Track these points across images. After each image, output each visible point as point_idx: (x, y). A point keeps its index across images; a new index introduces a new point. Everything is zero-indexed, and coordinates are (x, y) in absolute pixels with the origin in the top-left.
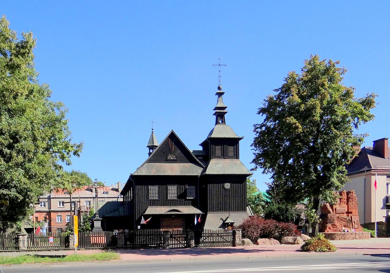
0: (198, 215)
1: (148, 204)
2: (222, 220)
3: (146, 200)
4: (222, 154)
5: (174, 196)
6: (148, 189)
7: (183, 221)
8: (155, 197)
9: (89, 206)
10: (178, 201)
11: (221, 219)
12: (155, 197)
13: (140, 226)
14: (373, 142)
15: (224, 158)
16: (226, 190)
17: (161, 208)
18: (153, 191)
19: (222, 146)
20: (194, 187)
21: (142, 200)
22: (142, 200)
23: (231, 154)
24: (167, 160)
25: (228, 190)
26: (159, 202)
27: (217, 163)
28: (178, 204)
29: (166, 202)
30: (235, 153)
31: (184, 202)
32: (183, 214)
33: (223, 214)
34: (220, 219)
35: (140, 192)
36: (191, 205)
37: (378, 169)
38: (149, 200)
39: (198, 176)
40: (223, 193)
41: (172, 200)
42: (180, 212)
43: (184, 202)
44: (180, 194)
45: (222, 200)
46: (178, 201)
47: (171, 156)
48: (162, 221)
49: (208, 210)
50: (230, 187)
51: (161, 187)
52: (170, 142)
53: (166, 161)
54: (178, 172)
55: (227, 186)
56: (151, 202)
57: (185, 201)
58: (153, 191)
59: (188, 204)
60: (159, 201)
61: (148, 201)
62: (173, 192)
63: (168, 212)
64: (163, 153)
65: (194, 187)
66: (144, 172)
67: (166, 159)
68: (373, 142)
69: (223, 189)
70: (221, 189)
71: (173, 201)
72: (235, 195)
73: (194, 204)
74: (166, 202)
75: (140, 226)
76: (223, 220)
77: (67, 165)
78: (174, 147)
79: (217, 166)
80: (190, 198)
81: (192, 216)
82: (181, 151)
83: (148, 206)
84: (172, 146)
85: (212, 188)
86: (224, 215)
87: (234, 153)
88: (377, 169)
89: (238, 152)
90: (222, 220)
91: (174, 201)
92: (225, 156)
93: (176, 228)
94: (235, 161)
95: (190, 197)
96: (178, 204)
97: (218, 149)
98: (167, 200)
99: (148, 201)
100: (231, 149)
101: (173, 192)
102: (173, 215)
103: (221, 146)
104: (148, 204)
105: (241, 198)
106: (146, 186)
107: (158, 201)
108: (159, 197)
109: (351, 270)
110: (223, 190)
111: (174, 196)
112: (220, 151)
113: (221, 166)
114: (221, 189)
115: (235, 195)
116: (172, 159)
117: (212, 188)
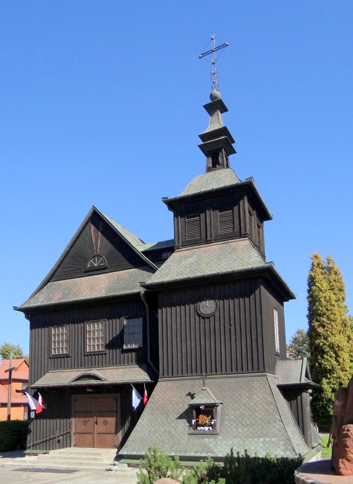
0: (139, 387)
5: (98, 345)
16: (203, 318)
28: (83, 364)
34: (187, 395)
37: (231, 236)
42: (100, 379)
45: (193, 344)
47: (94, 261)
54: (103, 291)
63: (76, 380)
66: (42, 300)
69: (196, 316)
77: (348, 309)
80: (129, 347)
84: (190, 216)
93: (101, 416)
95: (131, 344)
102: (90, 386)
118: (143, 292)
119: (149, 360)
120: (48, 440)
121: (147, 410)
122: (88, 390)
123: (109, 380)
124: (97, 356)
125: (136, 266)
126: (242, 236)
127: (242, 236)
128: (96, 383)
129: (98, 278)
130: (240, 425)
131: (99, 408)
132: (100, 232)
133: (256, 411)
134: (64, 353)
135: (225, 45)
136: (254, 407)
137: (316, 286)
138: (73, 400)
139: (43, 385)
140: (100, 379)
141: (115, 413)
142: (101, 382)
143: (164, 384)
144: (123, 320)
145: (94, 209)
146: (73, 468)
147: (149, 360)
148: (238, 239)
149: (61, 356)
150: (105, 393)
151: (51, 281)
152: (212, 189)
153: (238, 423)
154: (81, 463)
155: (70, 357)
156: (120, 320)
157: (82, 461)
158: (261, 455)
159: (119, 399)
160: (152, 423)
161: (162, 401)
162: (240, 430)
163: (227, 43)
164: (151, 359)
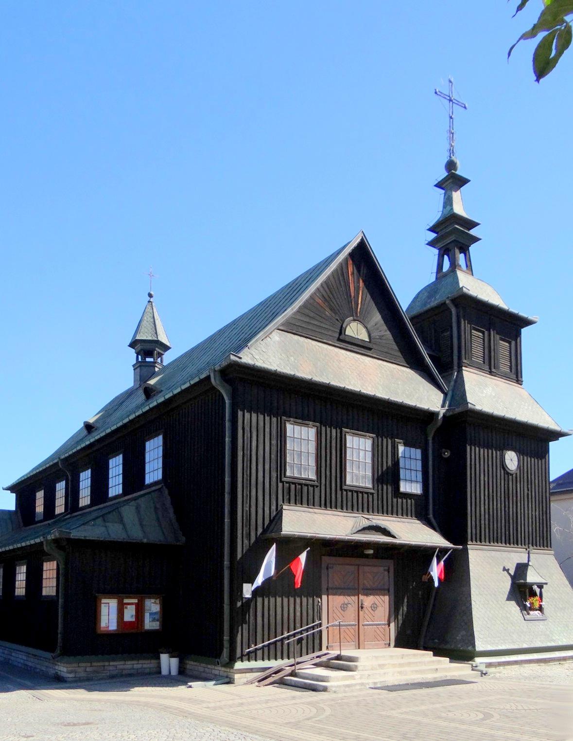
3: (274, 479)
6: (282, 436)
7: (389, 572)
11: (504, 569)
16: (508, 474)
17: (328, 516)
26: (317, 490)
28: (376, 509)
29: (339, 492)
31: (390, 501)
36: (413, 515)
38: (345, 487)
41: (358, 492)
42: (394, 537)
43: (390, 501)
44: (380, 473)
52: (353, 274)
53: (339, 340)
56: (293, 486)
57: (395, 500)
60: (317, 486)
65: (419, 452)
69: (502, 469)
70: (499, 471)
71: (355, 495)
72: (528, 494)
74: (339, 492)
78: (363, 297)
83: (280, 502)
87: (511, 364)
88: (349, 623)
91: (357, 492)
92: (492, 367)
96: (376, 509)
98: (341, 489)
99: (280, 485)
108: (318, 472)
109: (320, 734)
110: (502, 471)
114: (499, 471)
115: (528, 494)
118: (442, 415)
119: (431, 516)
122: (371, 552)
123: (403, 539)
125: (412, 367)
138: (324, 565)
139: (326, 536)
140: (394, 537)
141: (387, 592)
144: (397, 445)
147: (431, 516)
149: (304, 482)
150: (370, 558)
152: (498, 306)
156: (278, 419)
158: (149, 688)
159: (392, 570)
164: (434, 516)
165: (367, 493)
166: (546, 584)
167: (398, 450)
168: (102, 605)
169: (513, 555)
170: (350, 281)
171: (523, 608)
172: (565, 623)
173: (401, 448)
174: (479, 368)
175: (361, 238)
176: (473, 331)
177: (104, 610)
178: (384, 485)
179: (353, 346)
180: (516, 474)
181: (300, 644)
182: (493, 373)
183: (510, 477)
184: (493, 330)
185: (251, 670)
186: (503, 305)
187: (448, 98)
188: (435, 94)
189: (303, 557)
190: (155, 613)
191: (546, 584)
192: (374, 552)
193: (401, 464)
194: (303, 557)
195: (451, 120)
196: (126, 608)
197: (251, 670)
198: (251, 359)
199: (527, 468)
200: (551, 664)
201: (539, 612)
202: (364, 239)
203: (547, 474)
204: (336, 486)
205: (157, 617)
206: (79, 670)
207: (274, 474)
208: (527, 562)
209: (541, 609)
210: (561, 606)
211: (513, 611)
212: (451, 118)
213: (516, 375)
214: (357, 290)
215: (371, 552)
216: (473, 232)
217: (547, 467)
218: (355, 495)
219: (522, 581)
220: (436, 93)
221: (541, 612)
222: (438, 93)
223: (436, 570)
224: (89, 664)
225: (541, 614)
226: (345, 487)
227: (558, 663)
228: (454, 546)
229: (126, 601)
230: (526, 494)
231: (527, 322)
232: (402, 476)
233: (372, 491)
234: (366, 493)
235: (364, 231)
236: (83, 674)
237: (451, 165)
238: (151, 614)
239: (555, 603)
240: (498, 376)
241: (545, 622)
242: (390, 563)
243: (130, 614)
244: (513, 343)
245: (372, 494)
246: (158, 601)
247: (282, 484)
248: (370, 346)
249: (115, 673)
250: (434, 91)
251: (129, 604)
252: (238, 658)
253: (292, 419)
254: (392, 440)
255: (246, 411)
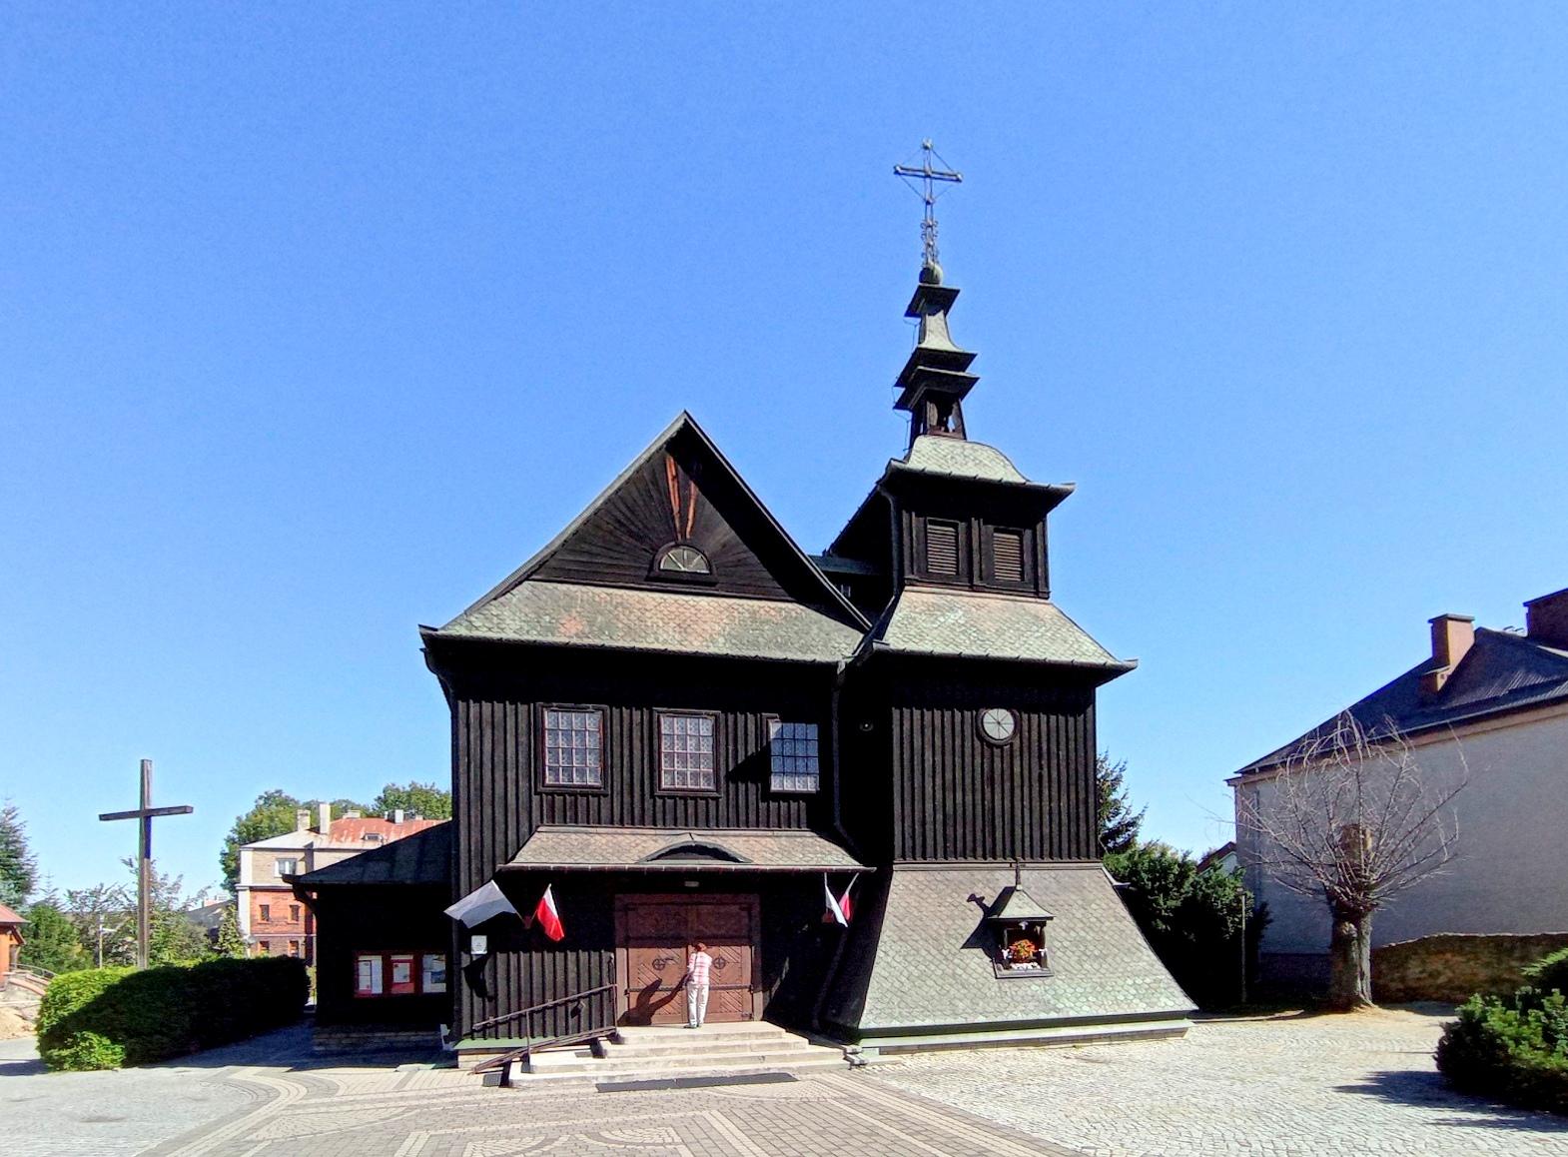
0: (839, 880)
1: (536, 814)
2: (979, 901)
4: (963, 565)
6: (537, 730)
8: (695, 775)
9: (1257, 770)
10: (722, 801)
11: (972, 898)
12: (582, 772)
13: (484, 938)
14: (1525, 604)
15: (972, 588)
16: (991, 746)
17: (621, 838)
18: (569, 741)
19: (962, 526)
20: (813, 731)
21: (499, 790)
22: (499, 790)
23: (1007, 571)
24: (652, 574)
25: (1001, 747)
27: (939, 608)
29: (648, 804)
30: (1028, 568)
31: (752, 808)
32: (407, 1031)
33: (978, 875)
35: (487, 747)
38: (541, 789)
39: (836, 665)
40: (978, 760)
42: (735, 860)
43: (752, 808)
45: (969, 798)
46: (722, 801)
48: (626, 909)
49: (898, 852)
50: (1014, 732)
51: (616, 721)
53: (648, 579)
55: (999, 723)
57: (763, 805)
58: (569, 741)
59: (786, 822)
61: (540, 794)
62: (689, 751)
63: (658, 858)
64: (631, 534)
65: (813, 731)
66: (512, 623)
67: (651, 569)
68: (1525, 604)
70: (968, 744)
71: (680, 803)
72: (1040, 776)
73: (818, 816)
74: (648, 804)
75: (484, 938)
76: (983, 907)
79: (942, 619)
81: (807, 885)
82: (736, 532)
85: (910, 725)
86: (990, 879)
87: (1022, 567)
89: (1040, 562)
90: (979, 901)
91: (694, 798)
94: (1033, 606)
97: (941, 541)
98: (652, 796)
99: (536, 799)
100: (1005, 544)
101: (689, 751)
102: (692, 874)
103: (955, 526)
104: (536, 814)
105: (934, 777)
106: (523, 708)
107: (597, 795)
110: (977, 743)
111: (695, 775)
112: (950, 553)
113: (962, 622)
114: (968, 744)
115: (1040, 776)
116: (683, 569)
117: (910, 725)
118: (844, 667)
120: (514, 1019)
121: (888, 933)
122: (694, 884)
123: (756, 862)
124: (593, 801)
126: (1040, 595)
127: (1040, 595)
128: (699, 867)
129: (691, 603)
130: (1085, 958)
131: (701, 927)
132: (693, 485)
133: (1105, 933)
134: (575, 783)
135: (954, 178)
136: (1098, 924)
137: (1075, 718)
140: (735, 860)
142: (733, 867)
143: (909, 876)
144: (542, 712)
145: (685, 420)
146: (758, 1070)
147: (837, 823)
148: (1033, 600)
151: (534, 577)
152: (923, 470)
153: (1080, 954)
154: (763, 1057)
155: (605, 796)
157: (467, 1098)
159: (756, 911)
160: (910, 959)
161: (916, 913)
162: (1086, 966)
163: (959, 176)
165: (705, 799)
166: (1051, 918)
167: (768, 732)
168: (361, 964)
169: (997, 874)
170: (671, 490)
171: (996, 957)
172: (1098, 980)
173: (774, 728)
174: (945, 584)
175: (682, 422)
176: (929, 526)
177: (363, 969)
178: (740, 784)
179: (676, 585)
180: (1011, 745)
181: (576, 1018)
182: (975, 588)
183: (997, 751)
184: (977, 519)
185: (488, 1051)
186: (1014, 478)
187: (923, 174)
188: (894, 176)
189: (548, 896)
190: (440, 973)
191: (1051, 918)
192: (684, 883)
193: (775, 748)
194: (548, 896)
195: (929, 207)
196: (396, 966)
197: (488, 1051)
198: (466, 627)
199: (1039, 733)
200: (1051, 1047)
201: (1036, 964)
202: (691, 423)
203: (1090, 743)
204: (642, 790)
205: (443, 976)
206: (331, 1041)
207: (523, 784)
208: (1014, 885)
209: (1039, 959)
210: (1097, 953)
211: (973, 965)
212: (928, 203)
213: (1034, 583)
214: (684, 501)
215: (694, 884)
216: (970, 372)
217: (1089, 726)
218: (680, 803)
219: (995, 917)
220: (897, 172)
221: (1039, 964)
222: (901, 171)
223: (839, 910)
224: (344, 1035)
225: (1039, 967)
226: (658, 793)
227: (1071, 1045)
228: (862, 867)
229: (394, 958)
230: (1035, 775)
231: (1053, 497)
232: (774, 768)
233: (715, 794)
234: (702, 798)
235: (688, 411)
236: (334, 1048)
237: (927, 274)
238: (433, 974)
239: (1082, 948)
240: (986, 590)
241: (1048, 981)
242: (755, 899)
243: (402, 973)
244: (1028, 533)
245: (716, 799)
246: (443, 957)
247: (538, 797)
248: (712, 579)
249: (383, 1046)
250: (893, 171)
251: (402, 961)
252: (466, 1035)
253: (555, 704)
254: (756, 716)
255: (507, 703)
